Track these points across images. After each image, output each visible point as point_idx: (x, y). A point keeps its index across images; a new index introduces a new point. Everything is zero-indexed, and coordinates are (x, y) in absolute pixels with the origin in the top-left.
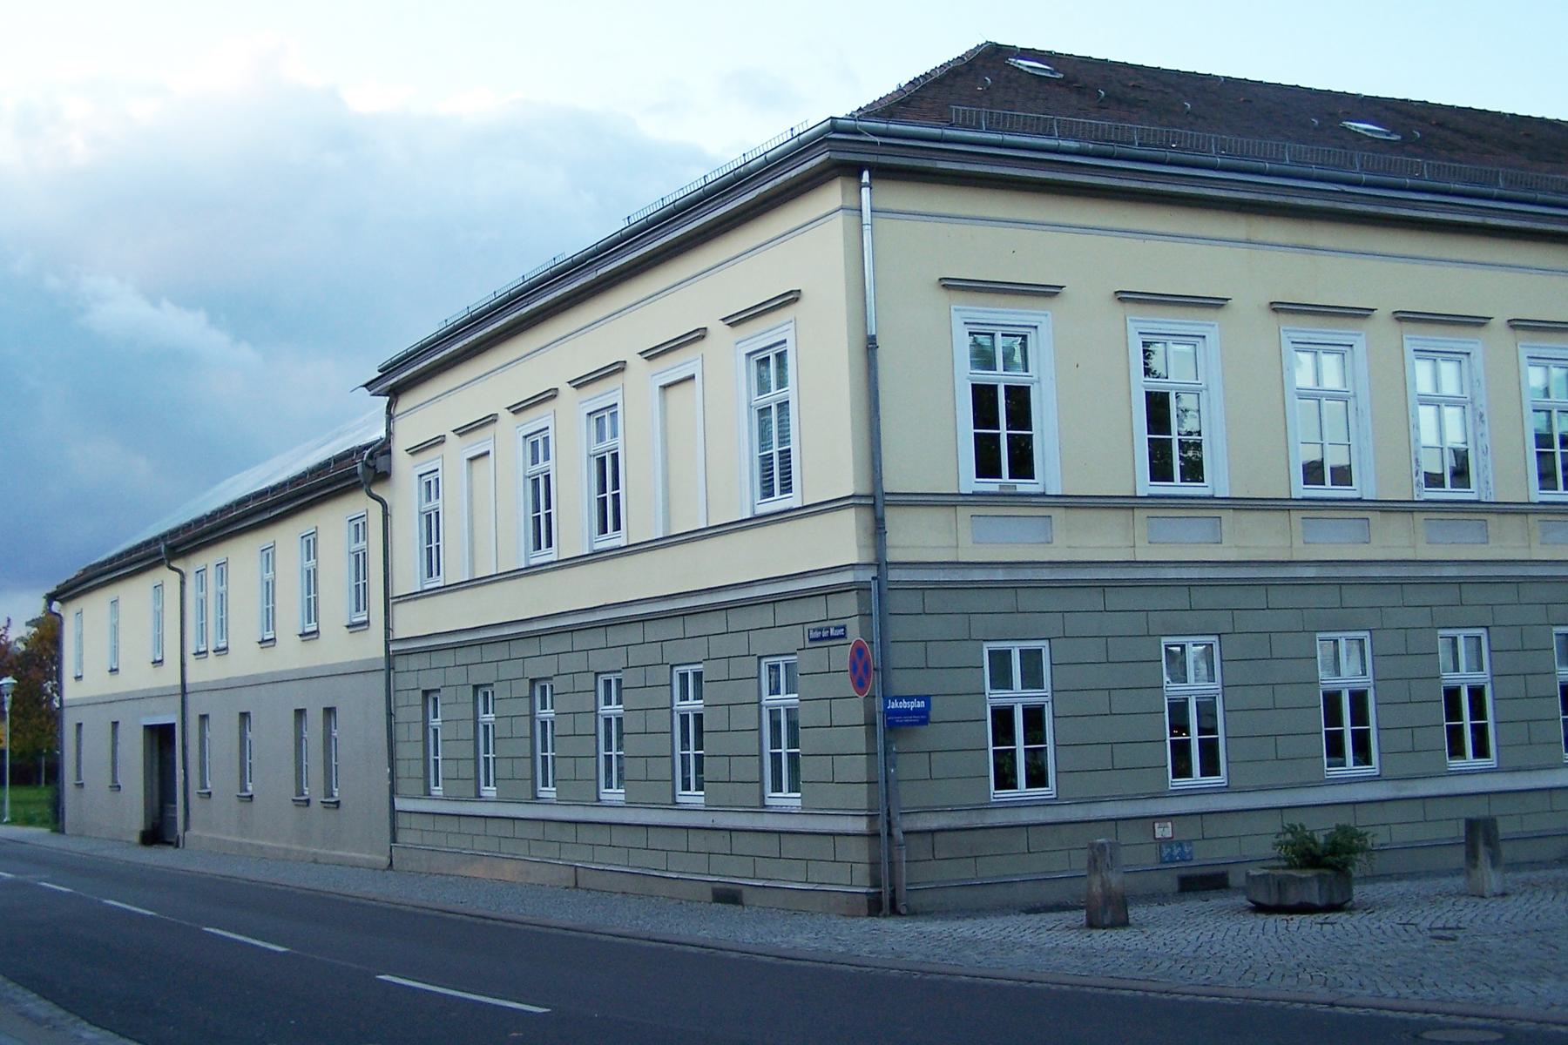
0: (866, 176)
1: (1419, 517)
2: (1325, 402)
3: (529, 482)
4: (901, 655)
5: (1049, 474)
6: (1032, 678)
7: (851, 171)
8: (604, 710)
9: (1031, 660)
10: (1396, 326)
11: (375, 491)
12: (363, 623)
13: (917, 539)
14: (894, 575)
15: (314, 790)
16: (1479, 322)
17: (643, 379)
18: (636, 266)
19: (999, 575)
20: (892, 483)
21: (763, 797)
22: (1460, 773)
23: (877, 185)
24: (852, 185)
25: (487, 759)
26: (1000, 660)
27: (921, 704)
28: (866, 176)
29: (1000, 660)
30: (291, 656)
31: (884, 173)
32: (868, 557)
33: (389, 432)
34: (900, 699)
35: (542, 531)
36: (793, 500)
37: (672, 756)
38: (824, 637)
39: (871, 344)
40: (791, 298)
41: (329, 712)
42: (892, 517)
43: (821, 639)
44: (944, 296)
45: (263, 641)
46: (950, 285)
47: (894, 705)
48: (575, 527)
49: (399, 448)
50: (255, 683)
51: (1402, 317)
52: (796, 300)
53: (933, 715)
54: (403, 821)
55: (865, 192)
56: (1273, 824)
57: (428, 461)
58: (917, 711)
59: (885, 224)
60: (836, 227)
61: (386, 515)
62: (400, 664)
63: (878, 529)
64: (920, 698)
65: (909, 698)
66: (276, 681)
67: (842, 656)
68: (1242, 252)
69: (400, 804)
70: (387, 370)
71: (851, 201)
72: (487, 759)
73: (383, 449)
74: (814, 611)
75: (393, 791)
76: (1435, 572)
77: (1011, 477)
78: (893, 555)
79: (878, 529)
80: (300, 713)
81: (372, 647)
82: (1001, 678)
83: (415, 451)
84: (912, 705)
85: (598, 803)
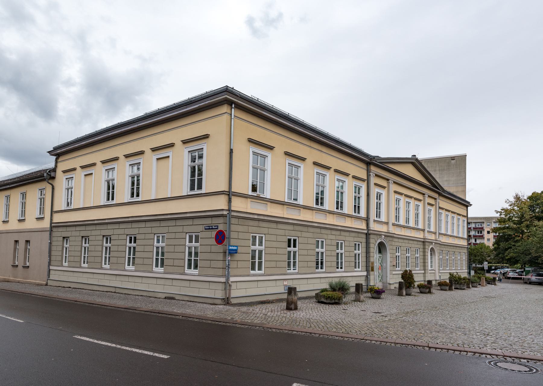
0: (233, 106)
2: (55, 209)
3: (106, 183)
6: (261, 244)
7: (230, 103)
8: (399, 254)
11: (50, 181)
12: (42, 218)
13: (238, 205)
14: (233, 214)
18: (173, 118)
19: (256, 217)
20: (234, 189)
24: (229, 107)
27: (236, 248)
28: (233, 106)
29: (254, 238)
32: (226, 208)
33: (56, 166)
34: (232, 246)
35: (110, 195)
36: (114, 202)
38: (209, 228)
39: (231, 151)
40: (206, 137)
42: (234, 199)
43: (209, 229)
45: (4, 221)
46: (251, 141)
47: (230, 248)
48: (123, 193)
52: (208, 137)
54: (51, 272)
55: (233, 109)
60: (226, 117)
61: (53, 188)
62: (54, 230)
63: (230, 201)
64: (236, 246)
65: (234, 246)
66: (8, 232)
67: (214, 233)
68: (309, 148)
69: (51, 268)
70: (55, 149)
71: (229, 111)
73: (54, 170)
74: (208, 221)
75: (49, 264)
78: (233, 209)
79: (230, 201)
80: (16, 242)
81: (46, 224)
83: (64, 172)
85: (102, 268)
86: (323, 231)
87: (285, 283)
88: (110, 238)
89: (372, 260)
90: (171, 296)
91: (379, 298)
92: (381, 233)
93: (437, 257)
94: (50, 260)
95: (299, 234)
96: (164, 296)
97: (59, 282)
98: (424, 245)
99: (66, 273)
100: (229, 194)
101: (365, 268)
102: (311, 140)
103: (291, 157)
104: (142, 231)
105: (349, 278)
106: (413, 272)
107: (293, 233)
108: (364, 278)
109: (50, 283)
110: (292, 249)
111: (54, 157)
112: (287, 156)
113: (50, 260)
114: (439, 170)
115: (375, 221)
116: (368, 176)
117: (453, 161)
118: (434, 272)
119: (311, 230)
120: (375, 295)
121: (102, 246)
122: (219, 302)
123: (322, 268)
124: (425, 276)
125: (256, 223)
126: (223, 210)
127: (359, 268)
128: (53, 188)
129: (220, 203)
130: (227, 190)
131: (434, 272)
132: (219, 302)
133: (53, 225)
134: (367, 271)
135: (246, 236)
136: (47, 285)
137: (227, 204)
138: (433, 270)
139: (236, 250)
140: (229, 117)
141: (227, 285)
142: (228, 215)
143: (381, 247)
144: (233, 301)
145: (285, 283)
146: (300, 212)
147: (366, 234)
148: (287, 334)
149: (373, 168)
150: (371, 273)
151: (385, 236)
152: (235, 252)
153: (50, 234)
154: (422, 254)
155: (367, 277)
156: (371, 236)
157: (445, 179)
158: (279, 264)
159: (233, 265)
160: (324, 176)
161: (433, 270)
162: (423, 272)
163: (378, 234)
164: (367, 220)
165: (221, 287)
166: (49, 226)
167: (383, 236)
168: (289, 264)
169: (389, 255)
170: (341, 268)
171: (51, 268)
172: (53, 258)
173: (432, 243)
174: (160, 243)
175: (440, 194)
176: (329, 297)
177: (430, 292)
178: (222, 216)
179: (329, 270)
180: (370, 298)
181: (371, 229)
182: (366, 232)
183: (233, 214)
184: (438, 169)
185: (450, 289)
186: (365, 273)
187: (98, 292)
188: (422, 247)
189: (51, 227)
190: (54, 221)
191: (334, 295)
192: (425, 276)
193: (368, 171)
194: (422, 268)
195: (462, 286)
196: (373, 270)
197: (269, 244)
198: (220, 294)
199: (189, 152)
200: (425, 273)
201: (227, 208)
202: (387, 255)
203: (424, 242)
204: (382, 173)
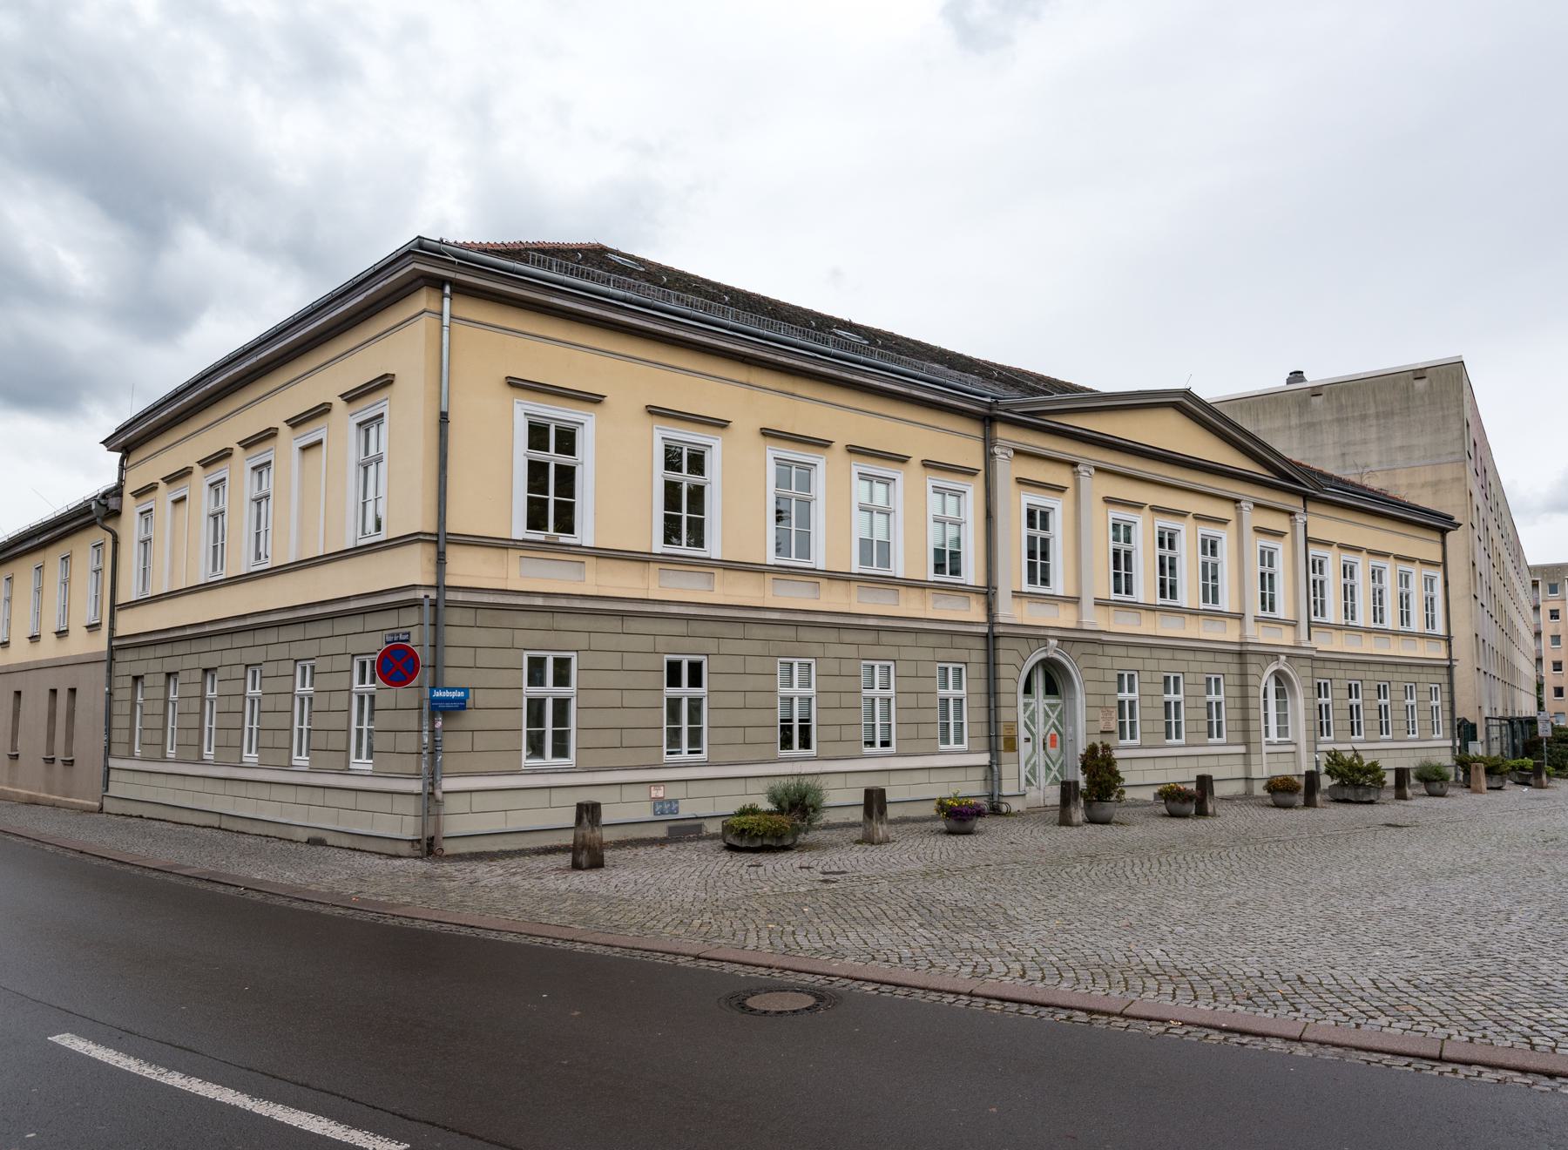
0: (447, 290)
1: (854, 585)
2: (121, 600)
4: (451, 657)
5: (586, 532)
6: (562, 679)
7: (437, 283)
8: (1221, 697)
9: (562, 666)
10: (847, 456)
11: (109, 525)
13: (466, 569)
14: (450, 596)
15: (60, 755)
16: (902, 460)
17: (290, 442)
19: (539, 601)
20: (453, 526)
21: (348, 761)
22: (535, 772)
23: (457, 298)
24: (436, 294)
25: (301, 731)
26: (537, 665)
27: (461, 694)
28: (447, 290)
30: (49, 649)
31: (461, 290)
33: (121, 479)
34: (444, 689)
37: (348, 731)
39: (444, 418)
40: (386, 381)
41: (73, 691)
42: (453, 553)
44: (509, 391)
47: (438, 694)
49: (127, 491)
50: (26, 669)
51: (853, 450)
53: (469, 703)
55: (447, 301)
56: (764, 785)
57: (147, 503)
58: (457, 700)
59: (456, 326)
61: (116, 542)
62: (119, 656)
63: (441, 560)
64: (460, 689)
66: (38, 667)
68: (743, 391)
69: (113, 763)
70: (121, 431)
71: (434, 307)
72: (301, 731)
76: (862, 622)
77: (556, 530)
78: (450, 581)
79: (441, 560)
80: (54, 692)
81: (100, 643)
82: (536, 678)
84: (453, 694)
86: (806, 634)
87: (659, 793)
88: (313, 667)
89: (1005, 715)
90: (320, 834)
91: (969, 833)
92: (1042, 632)
93: (1301, 702)
94: (109, 741)
95: (711, 646)
96: (303, 835)
97: (123, 803)
98: (1243, 664)
99: (138, 778)
100: (440, 541)
101: (984, 742)
102: (749, 364)
103: (671, 421)
104: (275, 653)
105: (828, 777)
106: (1116, 754)
107: (1173, 665)
108: (980, 774)
109: (109, 805)
110: (549, 691)
111: (118, 455)
112: (656, 418)
113: (109, 741)
114: (1377, 416)
115: (1018, 595)
116: (989, 457)
117: (1419, 384)
118: (1291, 748)
119: (757, 631)
120: (953, 824)
121: (243, 695)
122: (405, 849)
123: (1132, 737)
124: (1247, 765)
125: (542, 620)
126: (414, 587)
127: (1219, 735)
128: (116, 542)
129: (412, 568)
130: (432, 528)
131: (1291, 748)
132: (405, 849)
133: (115, 643)
134: (990, 750)
135: (506, 658)
136: (101, 810)
137: (432, 568)
138: (1289, 743)
139: (463, 700)
140: (435, 322)
141: (431, 800)
142: (438, 603)
143: (1054, 678)
144: (450, 848)
145: (659, 793)
146: (711, 582)
147: (986, 636)
148: (422, 933)
149: (1002, 432)
150: (1005, 756)
151: (1061, 640)
152: (456, 705)
153: (110, 670)
154: (1235, 692)
155: (992, 772)
156: (1002, 643)
157: (1398, 443)
158: (848, 733)
159: (450, 742)
160: (807, 468)
161: (1289, 743)
162: (1242, 749)
163: (1035, 636)
164: (988, 593)
165: (411, 806)
166: (105, 647)
167: (1053, 642)
168: (674, 735)
169: (1080, 699)
170: (885, 744)
171: (113, 763)
172: (115, 738)
173: (1275, 656)
174: (368, 684)
175: (1306, 498)
176: (743, 831)
177: (1202, 812)
178: (416, 604)
179: (832, 750)
180: (940, 832)
181: (1001, 620)
182: (985, 630)
183: (450, 596)
184: (1372, 411)
185: (1310, 803)
186: (984, 759)
187: (157, 824)
188: (1235, 669)
189: (112, 650)
190: (119, 633)
191: (782, 826)
192: (1247, 765)
193: (989, 443)
194: (1238, 738)
195: (1361, 791)
196: (1012, 745)
197: (592, 679)
198: (409, 829)
199: (359, 425)
200: (1246, 754)
201: (432, 581)
202: (1074, 700)
203: (1242, 654)
204: (1037, 443)
